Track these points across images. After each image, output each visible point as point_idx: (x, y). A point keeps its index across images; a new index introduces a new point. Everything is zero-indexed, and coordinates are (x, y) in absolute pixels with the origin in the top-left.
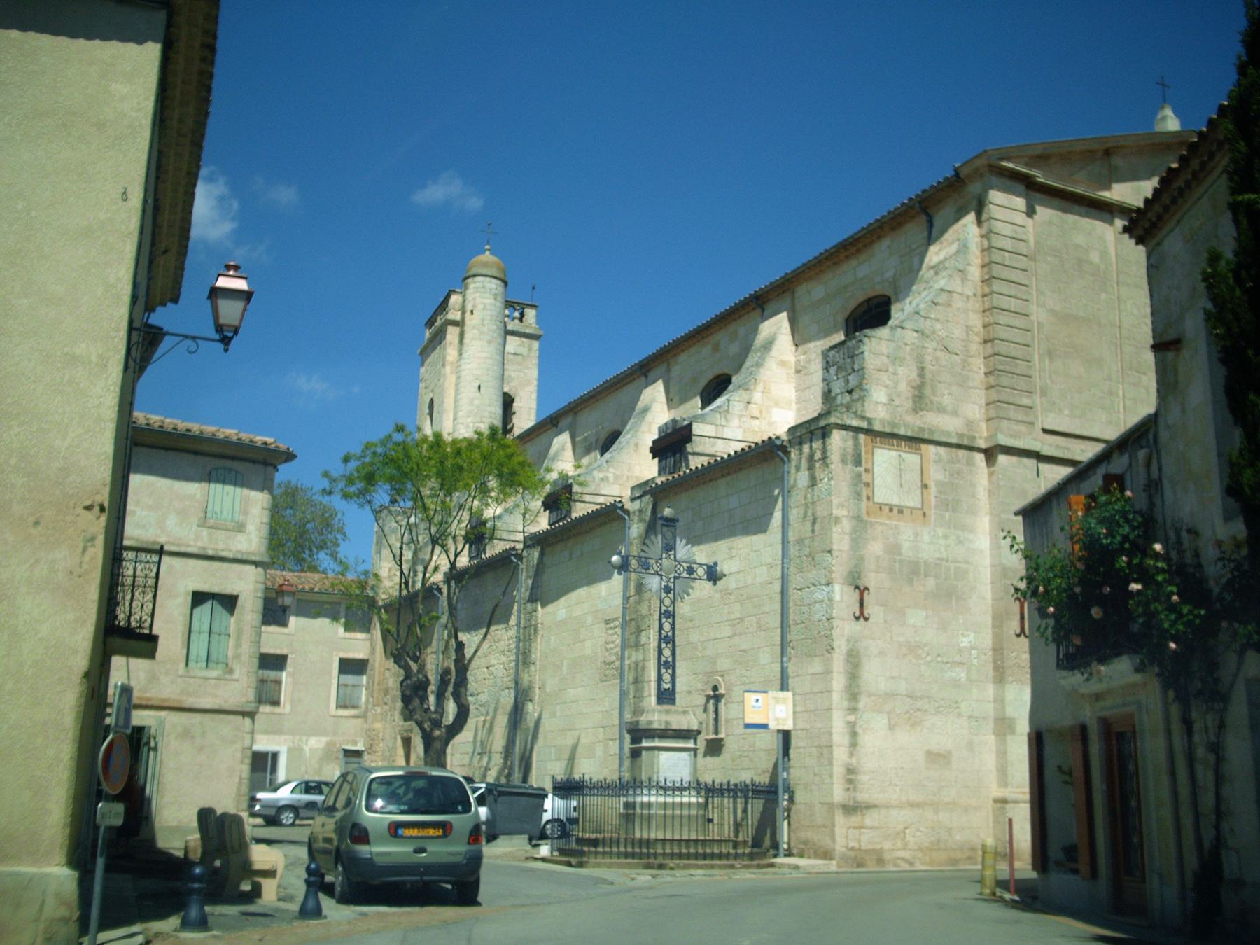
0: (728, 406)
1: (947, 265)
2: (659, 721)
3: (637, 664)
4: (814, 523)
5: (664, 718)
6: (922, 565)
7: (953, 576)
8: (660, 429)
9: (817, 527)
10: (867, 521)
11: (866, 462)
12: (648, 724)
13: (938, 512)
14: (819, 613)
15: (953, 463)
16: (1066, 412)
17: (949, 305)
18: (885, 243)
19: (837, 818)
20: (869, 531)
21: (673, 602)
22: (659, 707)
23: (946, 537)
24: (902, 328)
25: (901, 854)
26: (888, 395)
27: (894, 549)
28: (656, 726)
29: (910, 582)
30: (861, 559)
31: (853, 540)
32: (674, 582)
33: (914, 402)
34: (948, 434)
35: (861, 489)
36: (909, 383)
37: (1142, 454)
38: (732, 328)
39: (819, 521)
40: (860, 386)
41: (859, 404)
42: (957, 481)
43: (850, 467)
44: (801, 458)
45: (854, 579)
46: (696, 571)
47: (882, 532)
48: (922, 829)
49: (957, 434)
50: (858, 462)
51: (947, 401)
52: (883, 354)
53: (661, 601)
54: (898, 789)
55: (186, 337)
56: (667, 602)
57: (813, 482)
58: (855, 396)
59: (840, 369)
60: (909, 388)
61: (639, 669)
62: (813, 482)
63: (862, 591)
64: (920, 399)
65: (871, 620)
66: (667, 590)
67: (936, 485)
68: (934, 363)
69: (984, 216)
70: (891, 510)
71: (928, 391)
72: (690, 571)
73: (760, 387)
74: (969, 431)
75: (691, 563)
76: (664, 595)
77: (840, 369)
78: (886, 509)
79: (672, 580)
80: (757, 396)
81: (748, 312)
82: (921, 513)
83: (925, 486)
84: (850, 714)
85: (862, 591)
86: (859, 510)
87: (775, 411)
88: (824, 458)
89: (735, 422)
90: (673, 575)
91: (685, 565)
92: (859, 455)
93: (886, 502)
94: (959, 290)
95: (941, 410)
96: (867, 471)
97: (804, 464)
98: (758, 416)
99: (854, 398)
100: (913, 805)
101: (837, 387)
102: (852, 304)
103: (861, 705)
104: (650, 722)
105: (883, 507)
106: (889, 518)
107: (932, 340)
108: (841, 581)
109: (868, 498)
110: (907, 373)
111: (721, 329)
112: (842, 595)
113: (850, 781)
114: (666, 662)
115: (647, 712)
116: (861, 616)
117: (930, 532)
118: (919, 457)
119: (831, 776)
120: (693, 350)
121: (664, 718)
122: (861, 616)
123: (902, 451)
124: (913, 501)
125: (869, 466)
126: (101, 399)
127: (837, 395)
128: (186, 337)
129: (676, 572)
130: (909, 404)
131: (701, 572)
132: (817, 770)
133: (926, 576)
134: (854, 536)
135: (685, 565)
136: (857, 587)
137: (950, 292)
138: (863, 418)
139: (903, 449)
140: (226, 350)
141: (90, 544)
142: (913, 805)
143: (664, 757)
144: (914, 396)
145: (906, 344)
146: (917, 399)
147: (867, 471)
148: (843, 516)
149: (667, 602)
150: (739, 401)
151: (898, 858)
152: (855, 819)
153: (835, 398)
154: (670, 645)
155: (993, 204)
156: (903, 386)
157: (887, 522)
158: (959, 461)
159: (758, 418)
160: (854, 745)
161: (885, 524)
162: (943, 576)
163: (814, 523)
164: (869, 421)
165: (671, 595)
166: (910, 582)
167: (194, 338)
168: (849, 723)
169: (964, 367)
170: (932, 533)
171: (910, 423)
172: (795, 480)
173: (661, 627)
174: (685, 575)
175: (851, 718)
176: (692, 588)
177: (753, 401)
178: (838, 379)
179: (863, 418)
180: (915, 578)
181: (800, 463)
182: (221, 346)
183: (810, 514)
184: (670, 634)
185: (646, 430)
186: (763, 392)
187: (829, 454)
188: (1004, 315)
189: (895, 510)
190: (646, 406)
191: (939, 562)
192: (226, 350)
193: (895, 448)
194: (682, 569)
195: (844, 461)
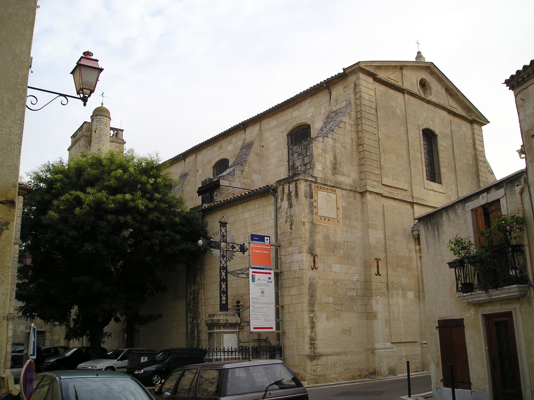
0: (234, 172)
1: (342, 110)
2: (223, 319)
3: (194, 291)
4: (291, 225)
5: (225, 318)
6: (338, 243)
7: (350, 249)
8: (203, 182)
9: (293, 227)
10: (316, 224)
11: (315, 197)
12: (218, 321)
13: (343, 220)
14: (295, 267)
15: (348, 198)
16: (391, 177)
17: (345, 128)
18: (307, 102)
19: (307, 362)
20: (317, 229)
21: (226, 262)
22: (221, 313)
23: (347, 232)
24: (327, 137)
25: (333, 376)
26: (323, 167)
27: (326, 237)
28: (222, 322)
29: (333, 251)
30: (314, 241)
31: (310, 233)
32: (226, 253)
33: (333, 170)
34: (346, 185)
35: (313, 209)
36: (330, 163)
37: (518, 189)
38: (229, 139)
39: (294, 224)
40: (310, 163)
41: (310, 171)
42: (350, 206)
43: (308, 199)
44: (284, 195)
45: (311, 251)
46: (235, 248)
47: (322, 229)
48: (341, 364)
49: (350, 185)
50: (312, 197)
51: (345, 171)
52: (320, 148)
53: (221, 262)
54: (331, 346)
55: (61, 95)
56: (223, 262)
57: (291, 205)
58: (308, 167)
59: (299, 154)
60: (331, 164)
61: (196, 294)
62: (291, 205)
63: (314, 256)
64: (335, 168)
65: (318, 269)
66: (223, 256)
67: (342, 208)
68: (340, 153)
69: (357, 91)
70: (329, 220)
71: (338, 166)
72: (233, 247)
73: (247, 164)
74: (354, 184)
75: (233, 244)
76: (222, 259)
77: (299, 154)
78: (323, 218)
79: (225, 252)
80: (246, 168)
81: (238, 131)
82: (337, 220)
83: (338, 208)
84: (310, 313)
85: (314, 256)
86: (313, 219)
87: (253, 175)
88: (297, 194)
89: (237, 180)
90: (225, 250)
91: (231, 245)
92: (312, 194)
93: (323, 215)
94: (348, 122)
95: (343, 175)
96: (315, 201)
97: (285, 198)
98: (247, 177)
99: (307, 168)
100: (338, 354)
101: (298, 163)
102: (290, 128)
103: (316, 309)
104: (219, 320)
105: (322, 217)
106: (325, 223)
107: (339, 143)
108: (306, 252)
109: (316, 214)
110: (329, 157)
111: (223, 139)
112: (306, 259)
113: (311, 344)
114: (223, 291)
115: (217, 315)
116: (314, 267)
117: (340, 229)
118: (335, 195)
119: (304, 342)
120: (209, 148)
121: (225, 318)
122: (314, 267)
123: (329, 192)
124: (333, 215)
125: (316, 199)
126: (11, 129)
127: (298, 166)
128: (61, 95)
129: (227, 248)
130: (330, 172)
131: (238, 248)
132: (295, 340)
133: (339, 249)
134: (311, 231)
135: (231, 245)
136: (312, 254)
137: (345, 122)
138: (313, 177)
139: (329, 191)
140: (85, 105)
141: (4, 227)
142: (338, 354)
143: (226, 336)
144: (333, 168)
145: (329, 145)
146: (334, 169)
147: (315, 201)
148: (306, 222)
149: (223, 262)
150: (239, 170)
151: (332, 378)
152: (315, 362)
153: (297, 168)
154: (225, 283)
155: (362, 85)
156: (328, 163)
157: (324, 224)
158: (351, 198)
159: (246, 178)
160: (313, 327)
161: (323, 225)
162: (346, 249)
163: (291, 225)
164: (316, 178)
165: (225, 259)
166: (333, 251)
167: (65, 96)
168: (310, 317)
169: (351, 156)
170: (341, 229)
171: (331, 179)
172: (280, 205)
173: (221, 275)
174: (231, 249)
175: (312, 315)
176: (234, 255)
177: (244, 170)
178: (298, 159)
179: (313, 177)
180: (335, 250)
181: (283, 197)
182: (81, 102)
183: (289, 221)
184: (225, 277)
185: (187, 184)
186: (248, 167)
187: (299, 193)
188: (367, 133)
189: (327, 219)
190: (186, 173)
191: (344, 243)
192: (85, 105)
193: (326, 191)
194: (229, 247)
195: (306, 196)
